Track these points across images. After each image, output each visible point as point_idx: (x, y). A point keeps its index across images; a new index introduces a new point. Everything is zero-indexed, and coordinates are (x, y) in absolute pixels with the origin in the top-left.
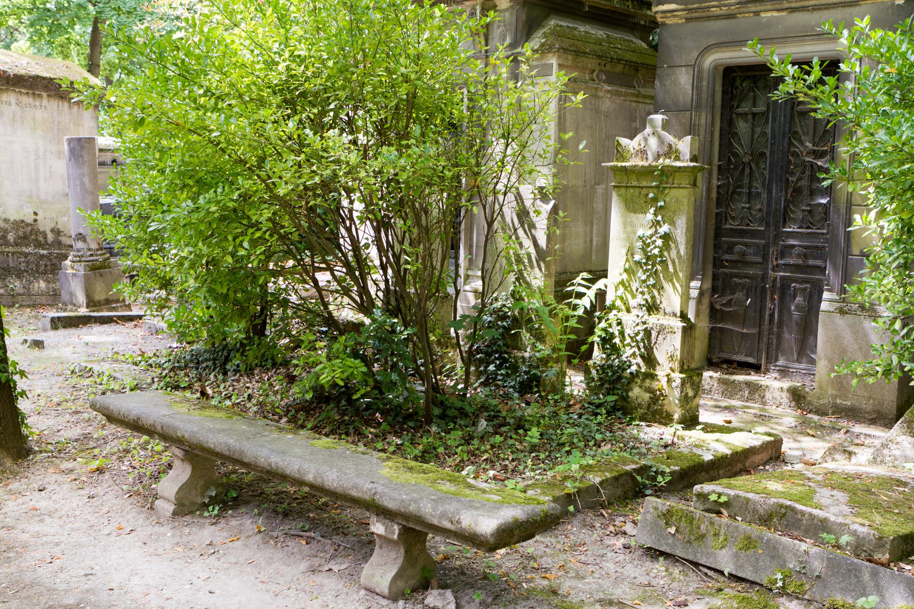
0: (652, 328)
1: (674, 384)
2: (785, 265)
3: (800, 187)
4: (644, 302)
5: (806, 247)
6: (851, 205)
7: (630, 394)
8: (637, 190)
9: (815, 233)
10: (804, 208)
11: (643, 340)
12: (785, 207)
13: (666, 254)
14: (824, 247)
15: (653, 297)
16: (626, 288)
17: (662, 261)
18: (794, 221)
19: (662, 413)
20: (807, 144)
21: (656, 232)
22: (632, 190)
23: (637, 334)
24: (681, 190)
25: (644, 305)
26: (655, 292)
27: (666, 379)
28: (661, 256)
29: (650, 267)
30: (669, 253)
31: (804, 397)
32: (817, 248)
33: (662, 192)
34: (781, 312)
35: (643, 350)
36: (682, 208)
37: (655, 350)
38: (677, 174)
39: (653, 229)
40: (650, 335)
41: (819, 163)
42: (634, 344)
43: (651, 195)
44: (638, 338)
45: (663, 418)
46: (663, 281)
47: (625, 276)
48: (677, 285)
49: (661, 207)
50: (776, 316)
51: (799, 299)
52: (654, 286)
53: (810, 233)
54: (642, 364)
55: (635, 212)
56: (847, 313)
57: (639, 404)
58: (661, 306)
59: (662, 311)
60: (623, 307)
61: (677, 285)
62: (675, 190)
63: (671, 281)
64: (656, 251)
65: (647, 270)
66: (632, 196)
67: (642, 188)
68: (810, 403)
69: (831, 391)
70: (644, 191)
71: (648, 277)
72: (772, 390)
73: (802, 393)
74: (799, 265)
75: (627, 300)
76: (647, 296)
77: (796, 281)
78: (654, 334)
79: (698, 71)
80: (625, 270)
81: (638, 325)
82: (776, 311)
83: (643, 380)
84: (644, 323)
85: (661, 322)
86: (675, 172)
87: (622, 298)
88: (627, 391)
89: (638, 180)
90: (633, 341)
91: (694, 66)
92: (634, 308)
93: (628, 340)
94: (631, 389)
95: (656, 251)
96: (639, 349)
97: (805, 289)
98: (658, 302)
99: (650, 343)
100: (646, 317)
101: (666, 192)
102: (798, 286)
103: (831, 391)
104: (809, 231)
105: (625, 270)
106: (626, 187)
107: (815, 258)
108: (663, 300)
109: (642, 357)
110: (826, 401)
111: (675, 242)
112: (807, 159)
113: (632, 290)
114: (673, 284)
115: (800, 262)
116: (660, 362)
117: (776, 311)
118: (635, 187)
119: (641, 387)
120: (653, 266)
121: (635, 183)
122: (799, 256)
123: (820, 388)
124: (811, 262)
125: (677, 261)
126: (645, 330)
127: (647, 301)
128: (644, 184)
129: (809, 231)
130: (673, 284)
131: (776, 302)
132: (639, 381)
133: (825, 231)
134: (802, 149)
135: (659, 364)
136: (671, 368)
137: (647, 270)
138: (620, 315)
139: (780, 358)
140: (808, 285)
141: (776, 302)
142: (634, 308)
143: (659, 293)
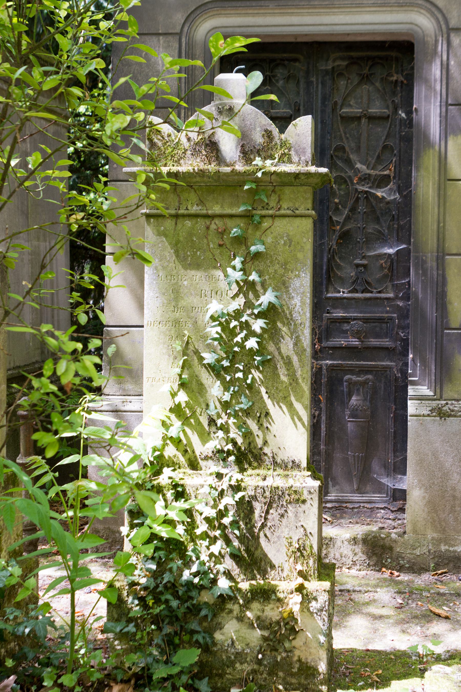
0: (254, 498)
1: (314, 605)
2: (334, 348)
3: (348, 231)
4: (230, 447)
5: (366, 320)
6: (444, 254)
7: (218, 636)
8: (201, 223)
9: (377, 298)
10: (358, 261)
11: (234, 523)
12: (329, 261)
13: (271, 347)
14: (391, 319)
15: (248, 435)
16: (185, 420)
17: (263, 363)
18: (342, 281)
19: (291, 665)
20: (358, 166)
21: (248, 305)
22: (188, 223)
23: (221, 514)
24: (298, 221)
25: (229, 453)
26: (252, 425)
27: (298, 598)
28: (261, 350)
29: (240, 375)
30: (277, 344)
31: (391, 549)
32: (381, 320)
33: (257, 226)
34: (330, 418)
35: (236, 543)
36: (300, 255)
37: (263, 541)
38: (287, 190)
39: (241, 300)
40: (251, 510)
41: (379, 194)
42: (218, 533)
43: (235, 231)
44: (226, 521)
45: (293, 675)
46: (269, 402)
47: (182, 397)
48: (298, 406)
49: (257, 255)
50: (323, 427)
51: (354, 400)
52: (248, 413)
53: (370, 299)
54: (236, 571)
55: (197, 266)
56: (450, 416)
57: (238, 654)
58: (267, 450)
59: (268, 461)
60: (182, 460)
61: (298, 406)
62: (285, 221)
63: (285, 399)
64: (252, 343)
65: (233, 382)
66: (190, 235)
67: (213, 217)
68: (400, 556)
69: (431, 534)
70: (216, 224)
71: (234, 395)
72: (339, 543)
73: (387, 542)
74: (355, 348)
75: (190, 443)
76: (234, 433)
77: (351, 371)
78: (258, 508)
79: (187, 44)
80: (183, 385)
81: (222, 494)
82: (324, 418)
83: (247, 605)
84: (236, 488)
85: (269, 482)
86: (284, 184)
87: (177, 442)
88: (210, 632)
89: (201, 202)
90: (213, 528)
91: (180, 34)
92: (206, 458)
93: (202, 528)
94: (220, 627)
95: (252, 343)
96: (228, 542)
97: (365, 383)
98: (259, 442)
99: (250, 529)
100: (237, 476)
101: (265, 224)
102: (354, 378)
103: (431, 534)
104: (368, 295)
105: (183, 385)
106: (177, 216)
107: (377, 336)
108: (270, 438)
109: (235, 557)
110: (424, 550)
111: (288, 321)
112: (361, 188)
113: (199, 423)
114: (290, 406)
115: (355, 342)
116: (275, 562)
117: (324, 418)
118: (196, 216)
119: (241, 619)
120: (246, 372)
121: (194, 209)
122: (357, 334)
123: (415, 531)
124: (374, 342)
125: (295, 359)
126: (240, 503)
127: (234, 443)
128: (217, 209)
129: (368, 295)
130: (290, 406)
131: (322, 405)
132: (236, 608)
133: (391, 295)
134: (351, 173)
135: (273, 567)
136: (301, 574)
137: (233, 382)
138: (177, 475)
139: (331, 488)
140: (370, 377)
141: (322, 405)
142: (206, 458)
143: (260, 426)
